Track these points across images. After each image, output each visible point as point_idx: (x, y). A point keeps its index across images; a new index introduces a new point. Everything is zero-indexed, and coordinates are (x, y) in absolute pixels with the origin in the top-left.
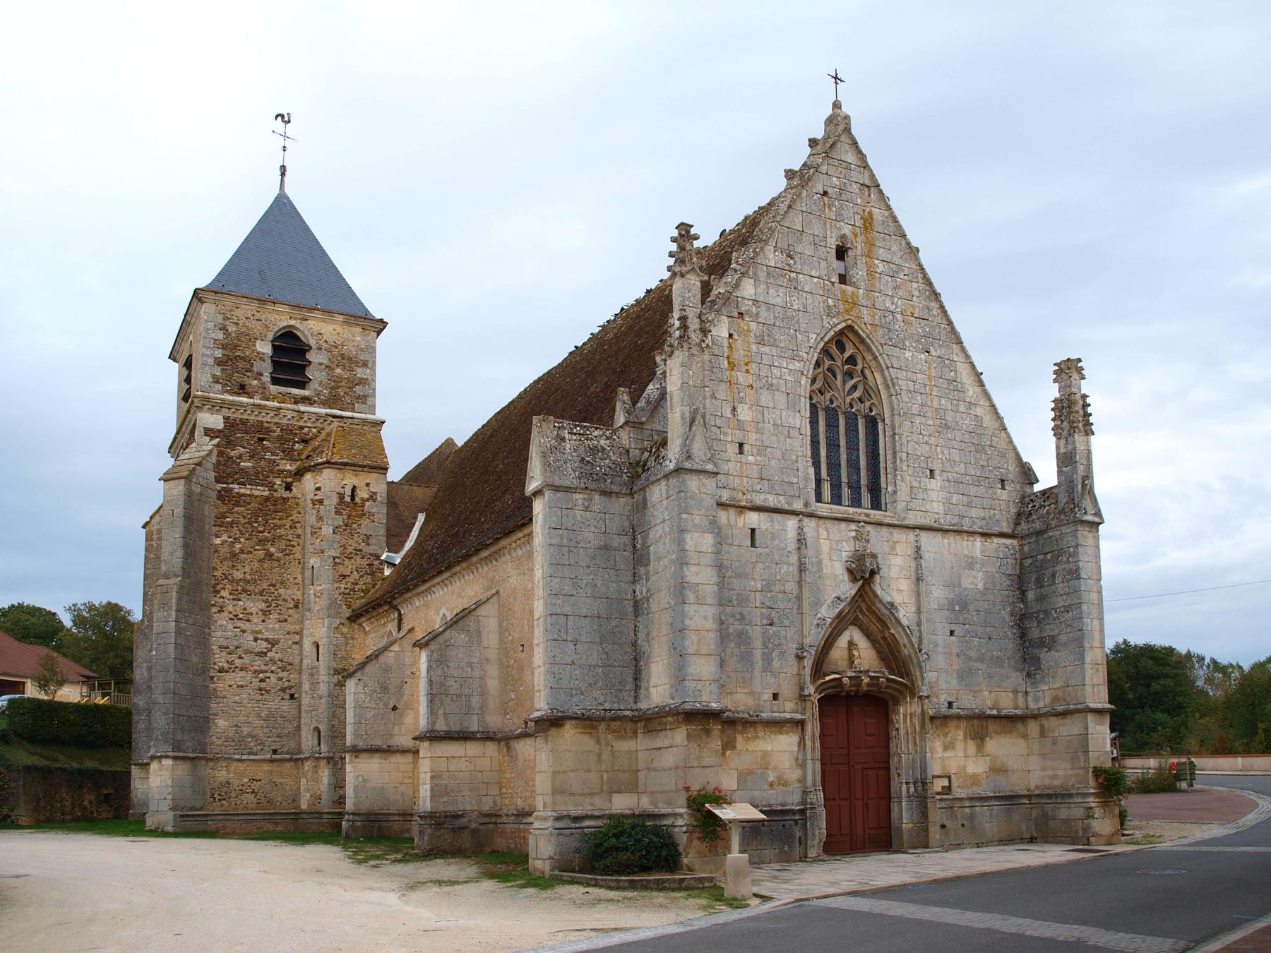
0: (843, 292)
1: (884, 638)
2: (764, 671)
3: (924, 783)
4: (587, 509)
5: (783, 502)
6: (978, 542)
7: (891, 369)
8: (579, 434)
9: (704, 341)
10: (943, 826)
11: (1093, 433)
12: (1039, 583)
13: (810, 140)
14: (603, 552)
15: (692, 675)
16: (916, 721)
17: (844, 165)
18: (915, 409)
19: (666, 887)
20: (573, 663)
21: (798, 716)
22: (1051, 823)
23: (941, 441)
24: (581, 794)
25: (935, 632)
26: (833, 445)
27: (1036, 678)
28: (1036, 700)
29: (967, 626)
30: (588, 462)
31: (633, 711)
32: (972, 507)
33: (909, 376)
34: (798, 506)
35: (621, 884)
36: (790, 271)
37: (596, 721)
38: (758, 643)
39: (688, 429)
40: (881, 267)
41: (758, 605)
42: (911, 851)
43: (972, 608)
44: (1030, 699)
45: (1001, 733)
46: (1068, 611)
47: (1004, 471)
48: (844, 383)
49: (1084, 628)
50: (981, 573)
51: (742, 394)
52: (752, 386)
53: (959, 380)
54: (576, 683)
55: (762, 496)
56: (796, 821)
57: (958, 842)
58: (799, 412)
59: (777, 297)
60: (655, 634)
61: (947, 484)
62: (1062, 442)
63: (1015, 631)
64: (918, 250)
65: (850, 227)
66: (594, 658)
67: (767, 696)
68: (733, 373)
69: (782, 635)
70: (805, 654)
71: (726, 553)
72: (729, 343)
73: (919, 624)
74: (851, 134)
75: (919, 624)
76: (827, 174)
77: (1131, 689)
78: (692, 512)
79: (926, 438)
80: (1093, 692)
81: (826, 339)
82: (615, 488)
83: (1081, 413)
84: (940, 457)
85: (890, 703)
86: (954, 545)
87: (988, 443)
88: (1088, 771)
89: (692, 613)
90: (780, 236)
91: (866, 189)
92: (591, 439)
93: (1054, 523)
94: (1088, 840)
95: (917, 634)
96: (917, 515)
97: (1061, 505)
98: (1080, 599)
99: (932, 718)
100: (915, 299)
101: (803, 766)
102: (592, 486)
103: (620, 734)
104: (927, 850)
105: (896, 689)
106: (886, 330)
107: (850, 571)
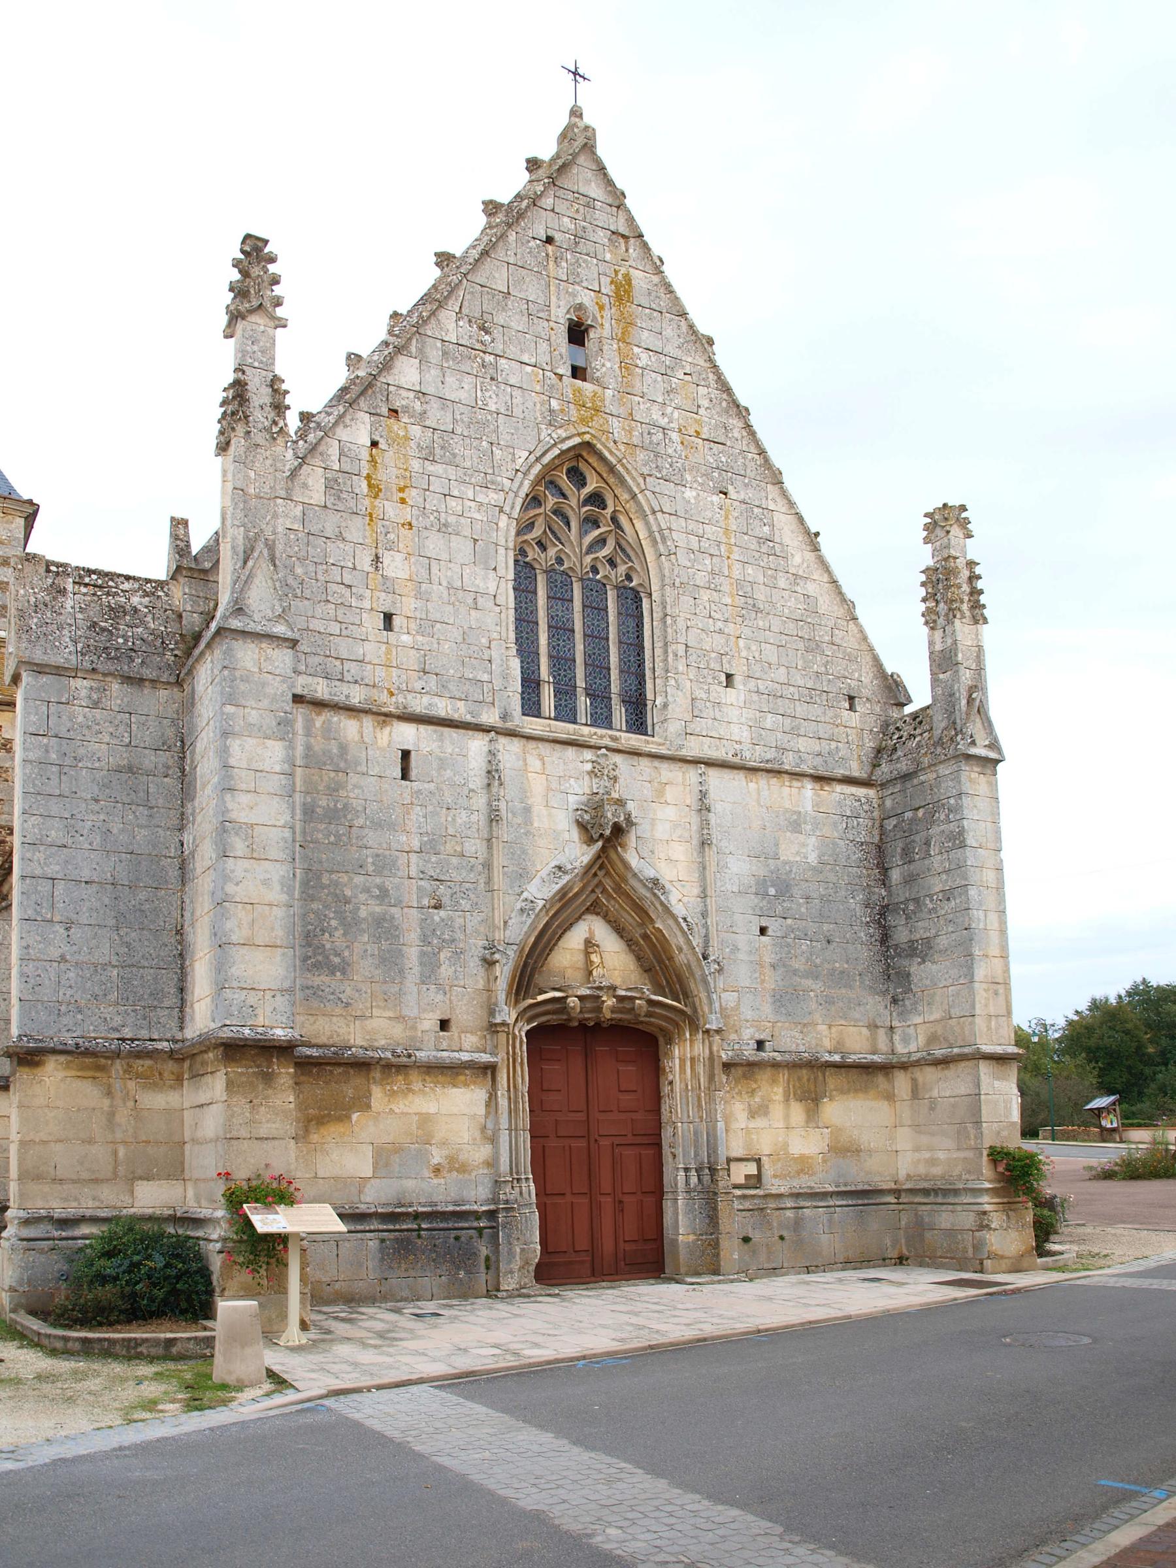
0: (579, 391)
1: (645, 937)
2: (423, 983)
3: (713, 1170)
4: (96, 705)
5: (463, 710)
6: (809, 789)
7: (659, 515)
8: (95, 586)
9: (275, 423)
10: (746, 1240)
11: (985, 621)
12: (907, 855)
13: (528, 161)
14: (124, 776)
15: (238, 979)
16: (700, 1069)
17: (583, 200)
18: (701, 578)
19: (141, 1353)
20: (63, 959)
21: (485, 1058)
22: (928, 1235)
23: (747, 632)
24: (74, 1182)
25: (734, 929)
26: (560, 629)
27: (904, 1005)
28: (906, 1040)
29: (789, 921)
30: (104, 630)
31: (176, 1041)
32: (799, 735)
33: (690, 528)
34: (490, 717)
35: (70, 1345)
36: (484, 352)
37: (107, 1058)
38: (412, 937)
39: (239, 564)
40: (644, 359)
41: (413, 874)
42: (689, 1280)
43: (797, 893)
44: (896, 1037)
45: (849, 1091)
46: (948, 899)
47: (853, 683)
48: (582, 534)
49: (973, 926)
50: (813, 839)
51: (391, 536)
52: (410, 524)
53: (777, 539)
54: (69, 992)
55: (426, 700)
56: (480, 1230)
57: (774, 1265)
58: (495, 569)
59: (459, 388)
60: (198, 913)
61: (755, 697)
62: (938, 634)
63: (871, 931)
64: (710, 342)
65: (592, 293)
66: (104, 953)
67: (430, 1023)
68: (377, 502)
69: (457, 926)
70: (497, 956)
71: (355, 786)
72: (371, 455)
73: (704, 915)
74: (594, 153)
75: (704, 915)
76: (553, 210)
77: (1151, 1041)
78: (243, 702)
79: (720, 624)
80: (989, 1028)
81: (547, 459)
82: (147, 673)
83: (966, 588)
84: (744, 654)
85: (661, 1040)
86: (766, 793)
87: (827, 638)
88: (981, 1154)
89: (239, 873)
90: (467, 297)
91: (621, 240)
92: (116, 594)
93: (926, 761)
94: (982, 1263)
95: (699, 931)
96: (702, 744)
97: (937, 733)
98: (966, 879)
99: (727, 1066)
100: (702, 411)
101: (493, 1140)
102: (111, 667)
103: (152, 1081)
104: (716, 1278)
105: (667, 1019)
106: (652, 455)
107: (582, 826)
